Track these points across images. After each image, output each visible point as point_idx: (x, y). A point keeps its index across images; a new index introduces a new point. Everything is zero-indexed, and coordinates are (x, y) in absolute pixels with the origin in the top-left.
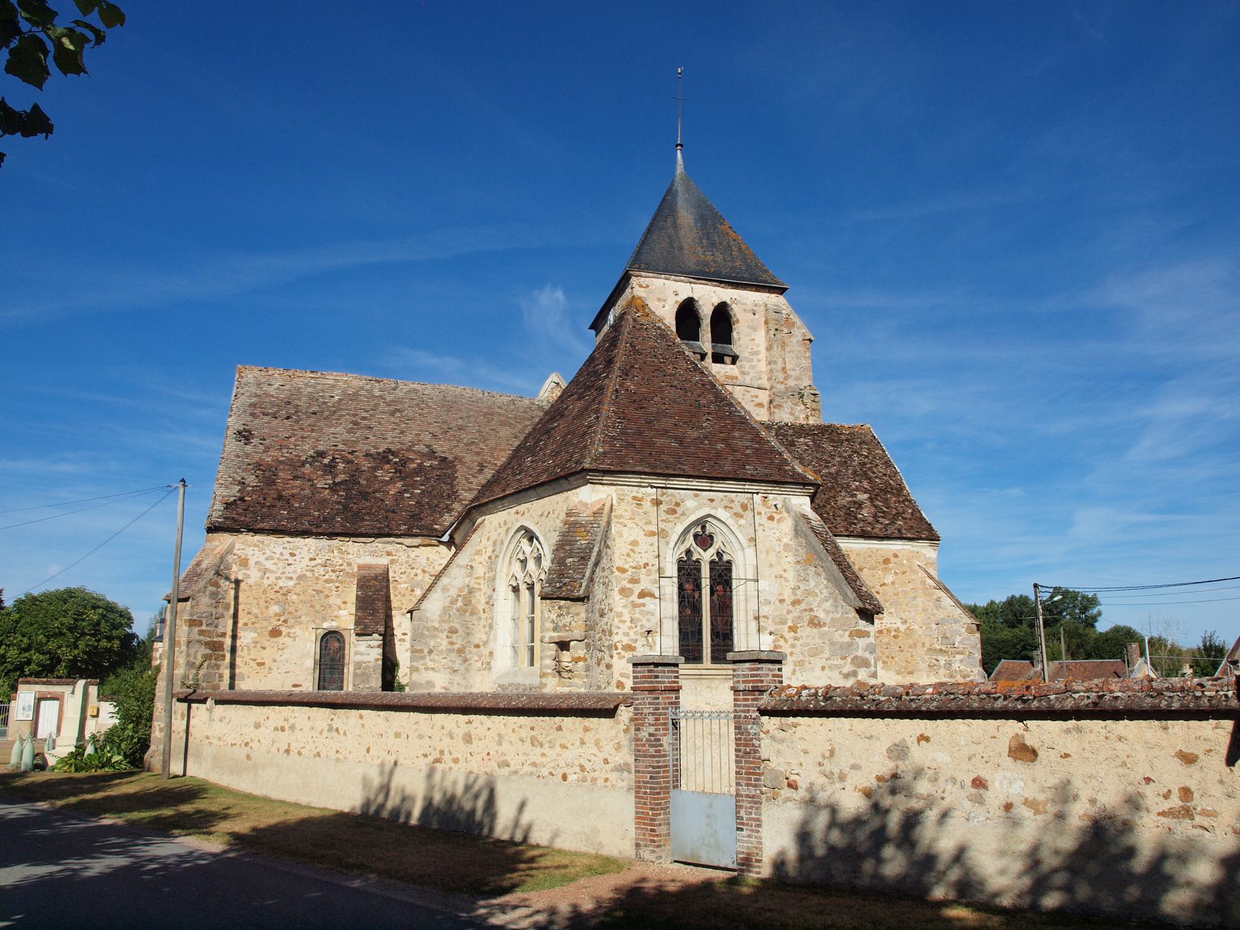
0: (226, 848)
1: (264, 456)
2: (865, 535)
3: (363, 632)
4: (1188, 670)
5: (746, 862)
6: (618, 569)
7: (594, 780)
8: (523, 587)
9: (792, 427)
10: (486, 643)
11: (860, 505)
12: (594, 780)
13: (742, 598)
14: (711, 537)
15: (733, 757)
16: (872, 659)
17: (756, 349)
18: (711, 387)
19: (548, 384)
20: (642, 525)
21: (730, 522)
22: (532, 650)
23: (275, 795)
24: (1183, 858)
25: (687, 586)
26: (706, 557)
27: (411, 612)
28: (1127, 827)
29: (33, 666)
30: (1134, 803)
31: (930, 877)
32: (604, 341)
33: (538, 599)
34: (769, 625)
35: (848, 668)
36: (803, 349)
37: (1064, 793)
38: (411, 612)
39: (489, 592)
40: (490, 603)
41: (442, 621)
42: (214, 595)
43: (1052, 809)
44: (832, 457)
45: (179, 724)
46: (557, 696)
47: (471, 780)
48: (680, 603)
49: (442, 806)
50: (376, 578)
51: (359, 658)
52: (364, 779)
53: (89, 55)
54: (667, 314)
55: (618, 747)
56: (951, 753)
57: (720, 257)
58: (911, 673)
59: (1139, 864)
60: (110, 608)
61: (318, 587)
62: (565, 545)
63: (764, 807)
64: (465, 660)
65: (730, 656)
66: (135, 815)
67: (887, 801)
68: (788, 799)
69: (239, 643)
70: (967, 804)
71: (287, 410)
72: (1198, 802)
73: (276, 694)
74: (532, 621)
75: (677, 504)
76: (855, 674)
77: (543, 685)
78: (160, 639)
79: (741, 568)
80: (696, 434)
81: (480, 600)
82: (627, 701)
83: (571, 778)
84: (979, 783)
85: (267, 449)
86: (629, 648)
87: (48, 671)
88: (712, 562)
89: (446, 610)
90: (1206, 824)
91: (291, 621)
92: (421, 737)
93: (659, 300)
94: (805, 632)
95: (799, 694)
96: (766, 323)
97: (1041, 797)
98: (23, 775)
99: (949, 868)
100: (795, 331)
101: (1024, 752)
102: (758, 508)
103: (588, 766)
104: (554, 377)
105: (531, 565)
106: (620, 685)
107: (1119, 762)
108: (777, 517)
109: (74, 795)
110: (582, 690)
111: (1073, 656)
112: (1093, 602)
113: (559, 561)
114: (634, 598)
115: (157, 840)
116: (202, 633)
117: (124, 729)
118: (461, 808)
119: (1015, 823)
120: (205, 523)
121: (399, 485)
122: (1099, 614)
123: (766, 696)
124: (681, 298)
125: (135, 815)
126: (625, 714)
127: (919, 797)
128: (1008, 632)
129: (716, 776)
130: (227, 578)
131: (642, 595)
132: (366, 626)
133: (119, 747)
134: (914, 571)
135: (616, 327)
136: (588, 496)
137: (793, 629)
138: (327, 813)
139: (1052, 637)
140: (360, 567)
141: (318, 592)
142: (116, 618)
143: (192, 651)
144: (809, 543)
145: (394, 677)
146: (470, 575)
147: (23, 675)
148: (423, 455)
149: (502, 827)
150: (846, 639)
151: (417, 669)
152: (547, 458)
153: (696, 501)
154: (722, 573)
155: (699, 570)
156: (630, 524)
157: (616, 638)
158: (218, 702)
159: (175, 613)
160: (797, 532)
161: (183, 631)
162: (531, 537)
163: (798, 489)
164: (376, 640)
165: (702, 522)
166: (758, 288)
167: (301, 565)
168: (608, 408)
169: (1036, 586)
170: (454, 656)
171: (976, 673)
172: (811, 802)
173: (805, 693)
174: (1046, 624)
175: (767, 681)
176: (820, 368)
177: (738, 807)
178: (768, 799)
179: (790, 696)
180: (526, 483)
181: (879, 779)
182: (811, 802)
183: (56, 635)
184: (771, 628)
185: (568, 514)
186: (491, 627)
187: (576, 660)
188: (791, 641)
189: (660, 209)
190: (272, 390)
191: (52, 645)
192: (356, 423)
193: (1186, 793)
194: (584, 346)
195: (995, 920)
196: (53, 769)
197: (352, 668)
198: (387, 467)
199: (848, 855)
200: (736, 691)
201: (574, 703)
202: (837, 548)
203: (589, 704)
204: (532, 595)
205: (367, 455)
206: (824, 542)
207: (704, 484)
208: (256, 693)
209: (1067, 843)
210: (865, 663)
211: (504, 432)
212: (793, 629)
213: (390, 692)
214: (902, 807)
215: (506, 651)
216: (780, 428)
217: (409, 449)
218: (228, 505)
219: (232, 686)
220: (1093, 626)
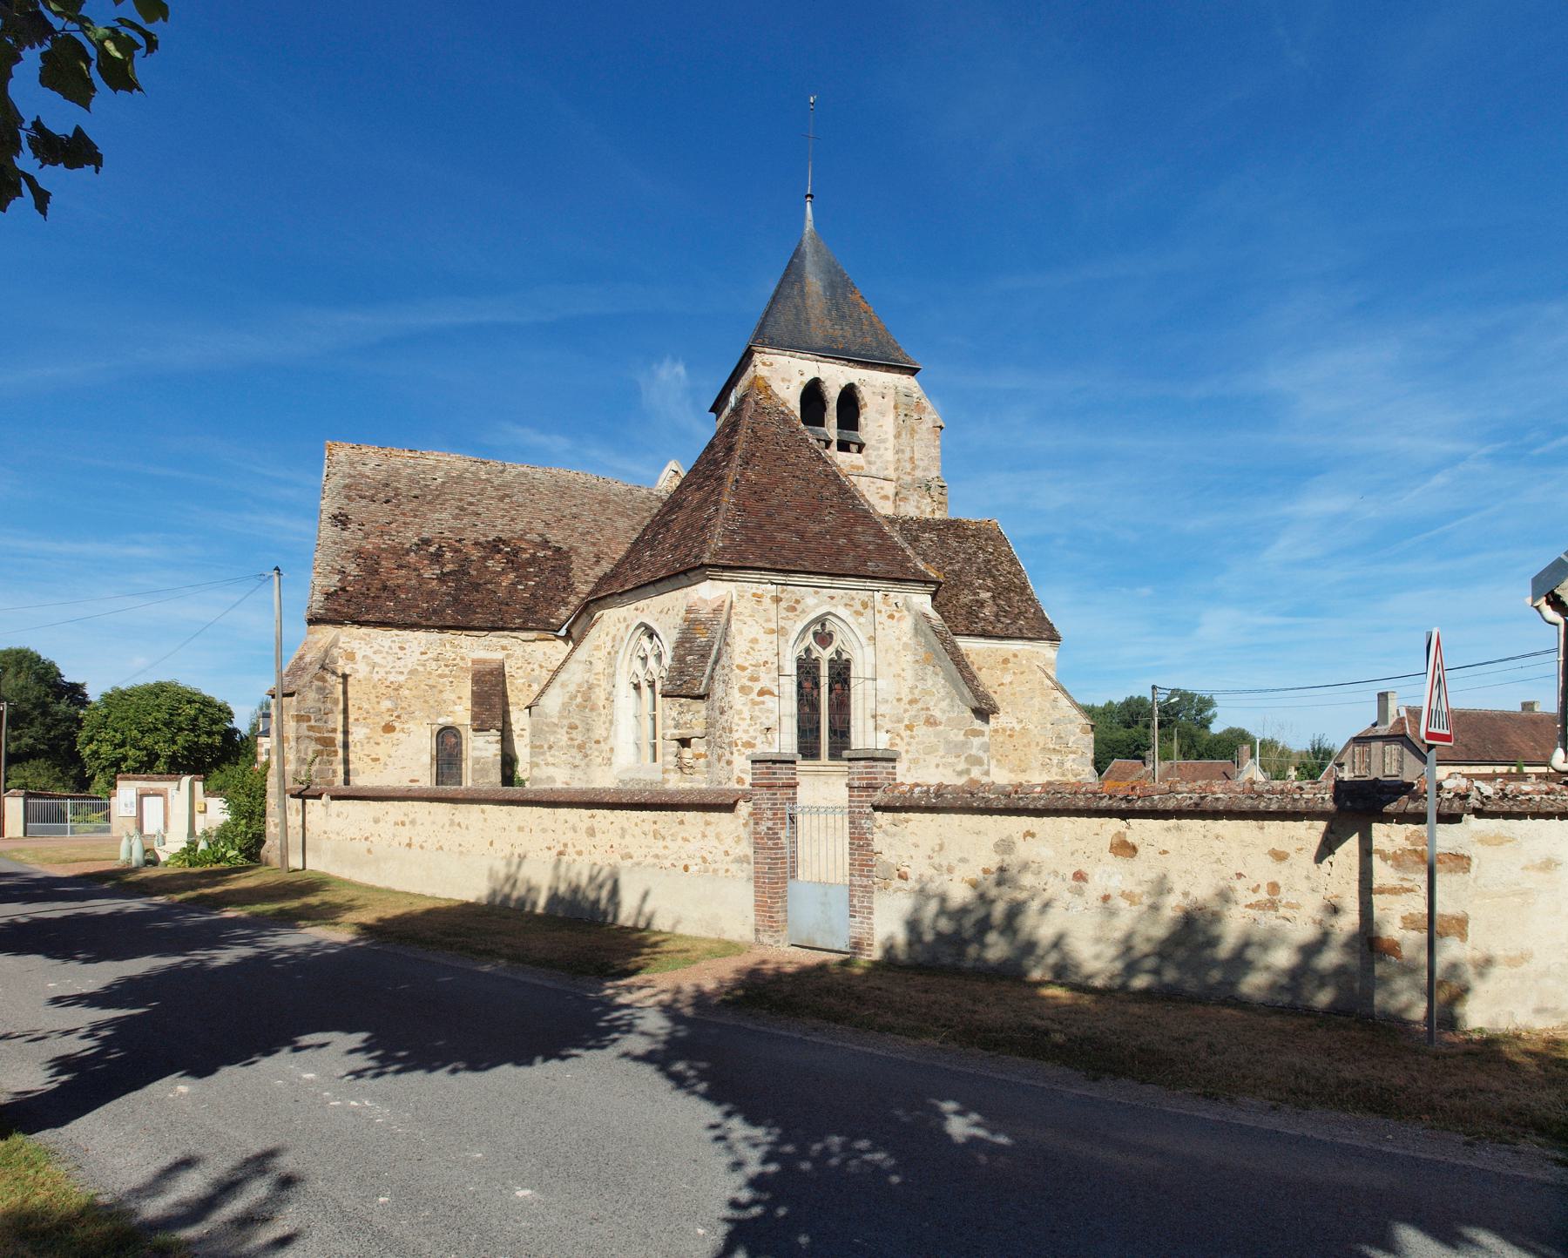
0: (354, 937)
1: (364, 543)
2: (985, 635)
3: (480, 729)
4: (1293, 773)
5: (857, 946)
6: (738, 667)
7: (715, 871)
8: (644, 685)
9: (918, 521)
10: (606, 739)
11: (981, 604)
12: (715, 871)
13: (860, 696)
14: (830, 635)
15: (847, 850)
16: (985, 757)
18: (834, 478)
19: (667, 473)
20: (764, 624)
21: (850, 620)
22: (654, 746)
23: (398, 887)
24: (1265, 946)
25: (806, 684)
26: (825, 655)
27: (529, 707)
28: (1216, 917)
29: (130, 763)
30: (1225, 896)
31: (1029, 962)
32: (724, 426)
33: (659, 697)
34: (886, 723)
35: (962, 766)
36: (932, 437)
37: (1161, 887)
38: (529, 707)
39: (609, 688)
40: (610, 699)
41: (561, 717)
42: (321, 690)
43: (1147, 901)
44: (956, 553)
45: (294, 820)
46: (678, 792)
47: (596, 869)
48: (799, 701)
49: (568, 896)
50: (491, 673)
51: (477, 754)
52: (491, 869)
53: (141, 66)
54: (790, 396)
55: (738, 840)
56: (1055, 846)
57: (849, 332)
59: (1225, 950)
60: (207, 703)
61: (431, 682)
62: (685, 642)
63: (876, 896)
64: (586, 756)
65: (846, 754)
66: (259, 908)
67: (993, 892)
68: (899, 889)
69: (351, 738)
70: (1068, 896)
71: (386, 492)
72: (1285, 896)
73: (394, 790)
74: (654, 719)
75: (797, 602)
76: (968, 771)
77: (665, 781)
78: (266, 733)
79: (860, 668)
80: (817, 529)
81: (599, 696)
82: (747, 797)
83: (691, 869)
84: (1079, 876)
85: (367, 536)
86: (749, 745)
87: (146, 766)
88: (831, 660)
89: (565, 706)
90: (1288, 915)
91: (404, 717)
92: (544, 830)
94: (921, 730)
95: (911, 791)
96: (896, 407)
97: (1138, 890)
98: (135, 870)
99: (1047, 953)
100: (925, 417)
101: (1125, 848)
102: (879, 606)
103: (709, 858)
104: (673, 465)
105: (652, 662)
106: (740, 781)
107: (1214, 858)
108: (897, 615)
109: (193, 889)
110: (704, 786)
111: (1185, 756)
112: (1207, 703)
113: (679, 659)
114: (754, 695)
115: (284, 931)
116: (311, 728)
117: (236, 825)
118: (586, 898)
119: (1112, 913)
120: (305, 615)
121: (512, 576)
122: (1215, 715)
123: (879, 793)
124: (807, 378)
125: (259, 908)
126: (744, 809)
127: (1021, 888)
128: (1124, 733)
129: (831, 866)
130: (334, 673)
131: (762, 693)
132: (483, 722)
133: (233, 842)
134: (1032, 671)
135: (737, 411)
136: (708, 593)
137: (909, 727)
138: (452, 904)
139: (1166, 737)
140: (474, 662)
141: (432, 687)
142: (215, 713)
143: (302, 747)
144: (928, 642)
145: (513, 772)
146: (590, 671)
147: (119, 771)
148: (536, 545)
149: (627, 914)
150: (961, 738)
151: (537, 765)
152: (667, 551)
153: (816, 598)
154: (841, 673)
155: (818, 668)
156: (749, 621)
157: (735, 736)
158: (333, 798)
159: (281, 709)
160: (917, 631)
161: (291, 727)
162: (651, 634)
163: (919, 587)
164: (494, 735)
165: (821, 620)
166: (889, 368)
167: (412, 659)
168: (727, 500)
169: (1154, 687)
170: (574, 751)
171: (1087, 774)
172: (922, 893)
173: (917, 790)
174: (1161, 725)
175: (881, 779)
176: (948, 458)
177: (852, 896)
178: (880, 889)
179: (904, 793)
180: (645, 578)
181: (986, 871)
182: (922, 893)
183: (150, 731)
184: (888, 727)
185: (688, 611)
186: (611, 722)
187: (698, 757)
188: (907, 740)
189: (786, 275)
190: (367, 470)
191: (148, 741)
192: (462, 509)
193: (1274, 887)
194: (706, 429)
195: (1086, 1000)
196: (166, 864)
197: (470, 763)
198: (498, 556)
199: (954, 941)
200: (851, 788)
201: (695, 799)
202: (956, 647)
203: (709, 799)
204: (654, 692)
205: (476, 544)
206: (943, 641)
207: (825, 581)
208: (372, 789)
209: (1160, 931)
210: (977, 761)
211: (622, 523)
212: (909, 727)
213: (509, 785)
214: (1006, 898)
215: (627, 750)
216: (905, 522)
217: (521, 538)
218: (328, 596)
219: (347, 782)
220: (1207, 727)
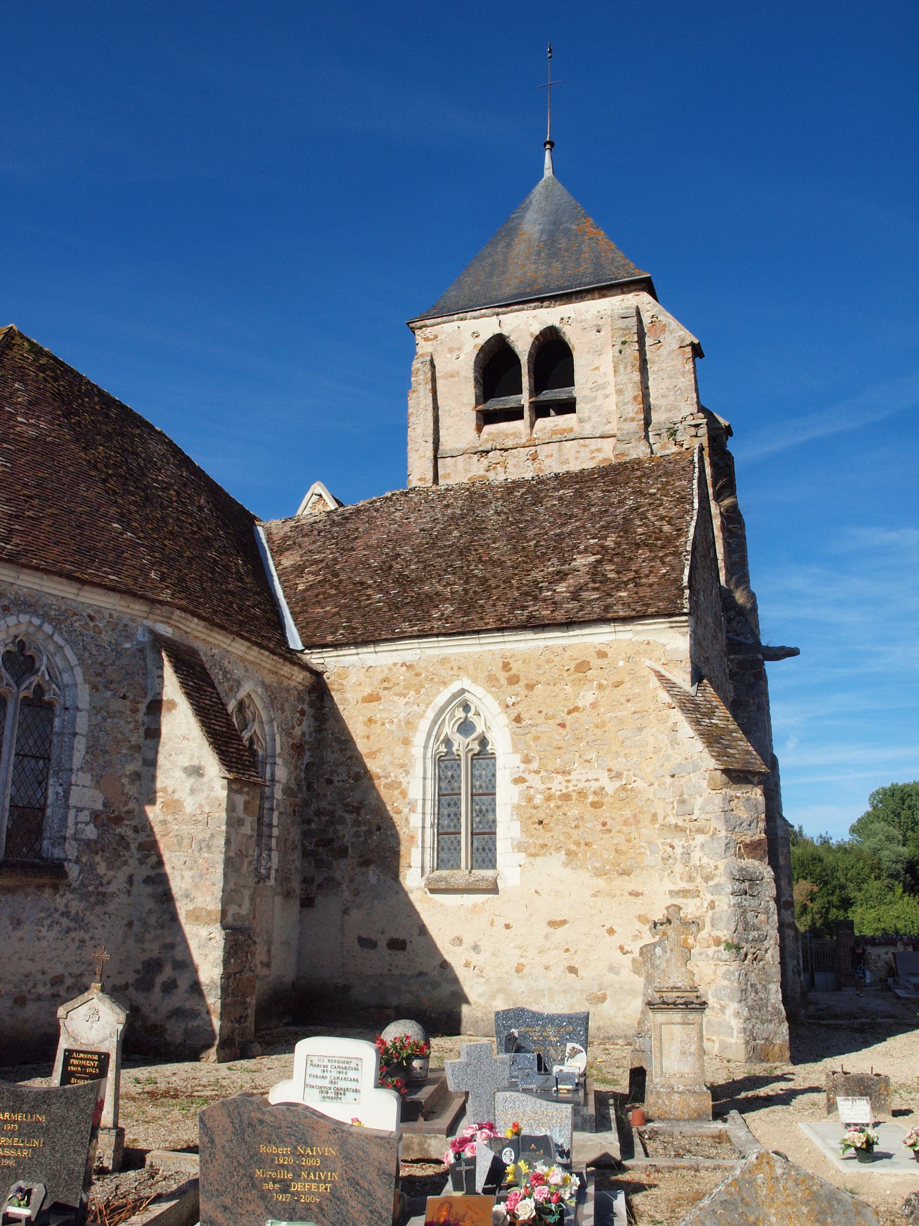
17: (600, 381)
58: (625, 873)
93: (451, 350)
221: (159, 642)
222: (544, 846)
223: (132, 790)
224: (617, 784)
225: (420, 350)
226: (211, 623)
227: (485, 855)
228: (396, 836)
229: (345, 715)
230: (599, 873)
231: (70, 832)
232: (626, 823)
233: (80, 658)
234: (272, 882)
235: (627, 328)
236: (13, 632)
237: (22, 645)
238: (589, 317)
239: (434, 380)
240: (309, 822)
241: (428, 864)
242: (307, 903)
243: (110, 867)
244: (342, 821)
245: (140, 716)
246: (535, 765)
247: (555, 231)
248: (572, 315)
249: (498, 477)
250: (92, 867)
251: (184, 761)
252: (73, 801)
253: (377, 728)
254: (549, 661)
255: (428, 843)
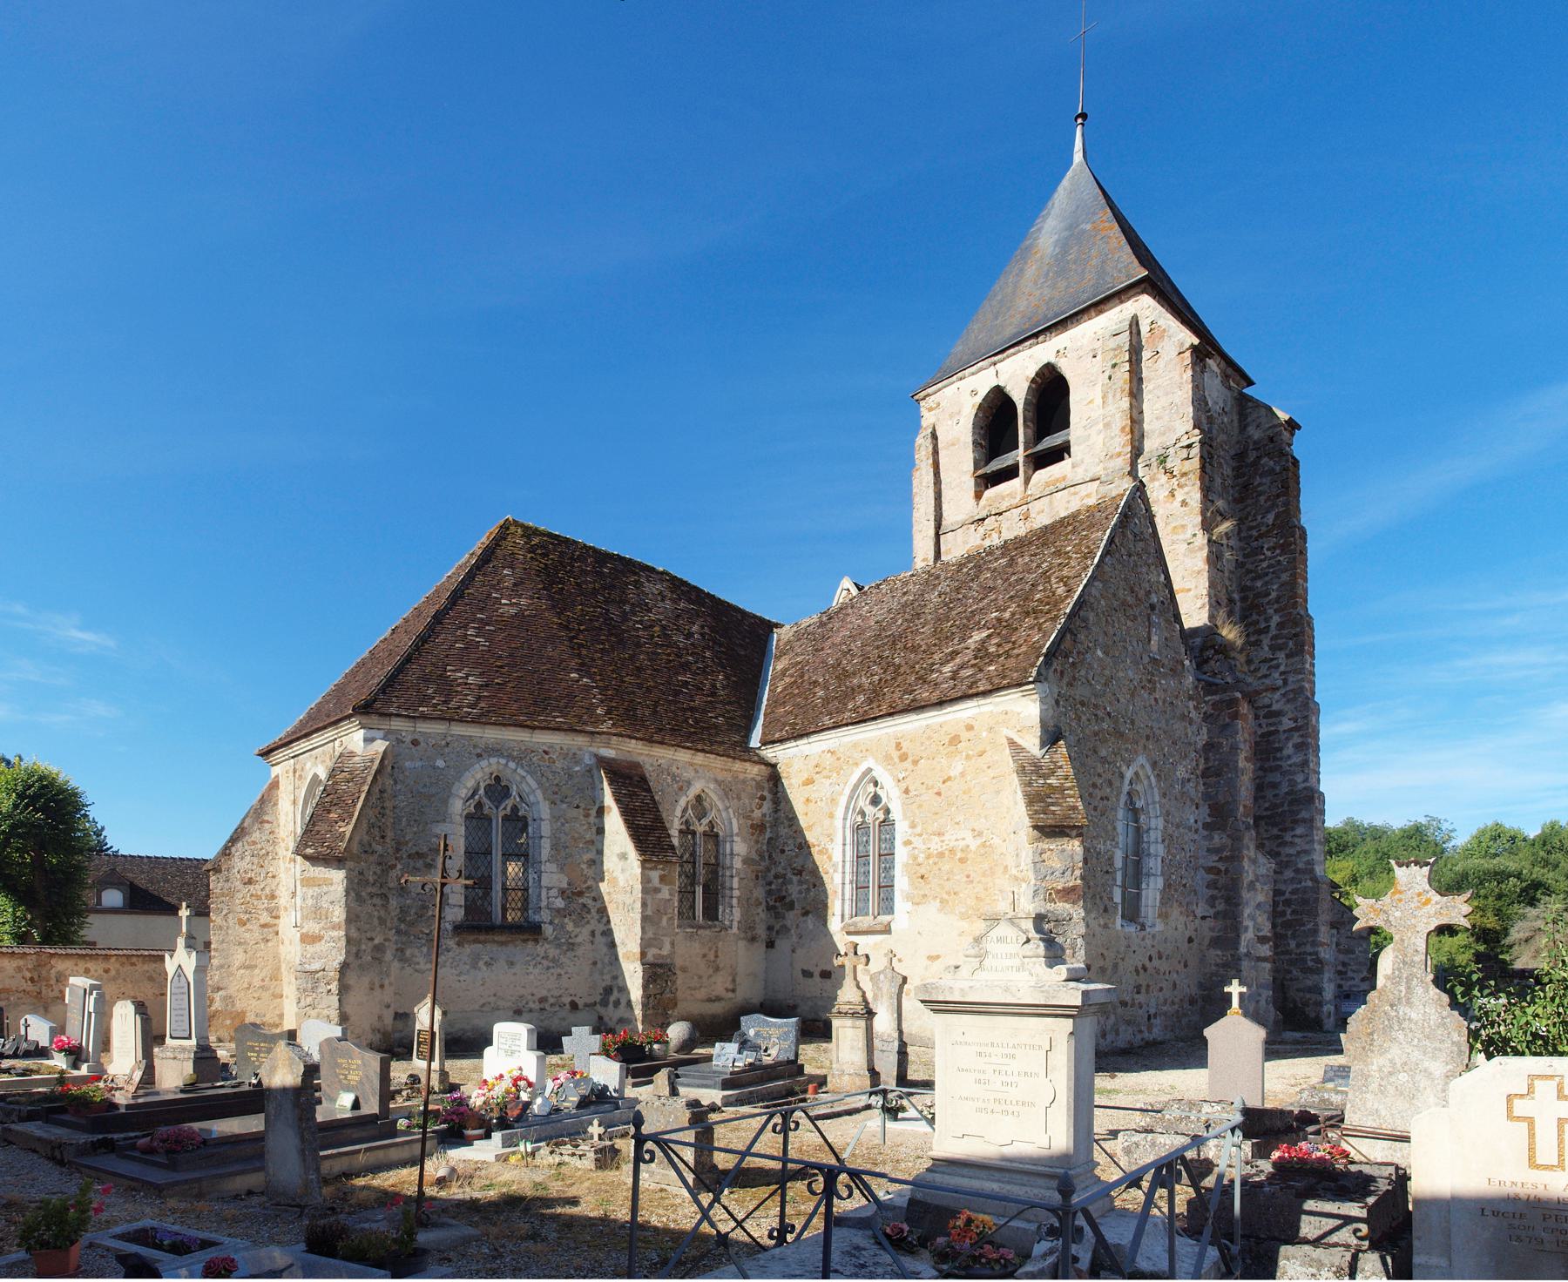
221: (603, 762)
222: (925, 896)
223: (590, 872)
224: (979, 841)
225: (924, 423)
226: (650, 741)
227: (887, 905)
228: (825, 892)
229: (791, 796)
230: (964, 916)
231: (543, 904)
232: (984, 875)
233: (540, 784)
234: (735, 930)
235: (1119, 347)
236: (487, 770)
237: (498, 779)
238: (1085, 341)
239: (936, 452)
240: (770, 884)
241: (847, 912)
242: (770, 945)
243: (576, 925)
244: (791, 882)
245: (592, 819)
246: (918, 830)
247: (1073, 236)
248: (1068, 344)
249: (995, 541)
250: (563, 926)
251: (618, 850)
252: (543, 883)
253: (812, 805)
254: (929, 738)
255: (847, 896)
